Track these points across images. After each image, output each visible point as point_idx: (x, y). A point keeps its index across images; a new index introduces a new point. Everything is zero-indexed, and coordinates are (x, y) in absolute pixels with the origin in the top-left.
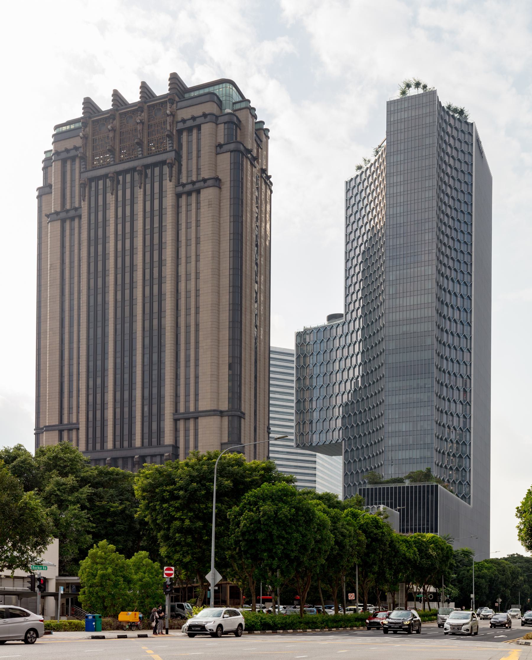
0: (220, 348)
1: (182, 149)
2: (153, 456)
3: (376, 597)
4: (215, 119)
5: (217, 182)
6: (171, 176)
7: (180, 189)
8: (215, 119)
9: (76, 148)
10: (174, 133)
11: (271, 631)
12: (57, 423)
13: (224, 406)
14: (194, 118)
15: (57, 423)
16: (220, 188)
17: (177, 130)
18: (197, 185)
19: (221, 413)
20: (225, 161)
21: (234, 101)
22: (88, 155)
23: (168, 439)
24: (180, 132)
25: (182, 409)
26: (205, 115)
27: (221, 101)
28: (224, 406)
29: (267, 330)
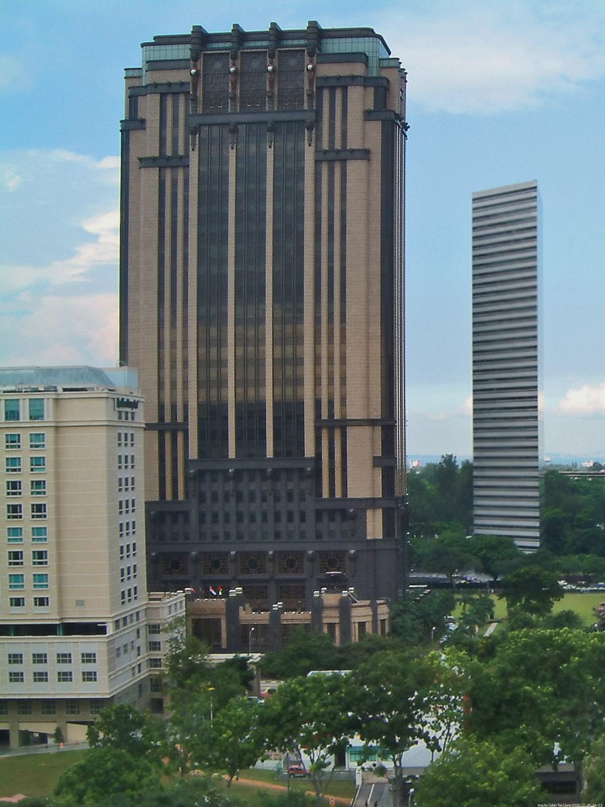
0: (370, 345)
1: (322, 107)
2: (289, 471)
3: (381, 597)
4: (365, 81)
5: (365, 154)
6: (310, 140)
7: (321, 156)
8: (365, 81)
9: (182, 84)
10: (315, 91)
11: (99, 625)
12: (156, 422)
13: (377, 414)
14: (339, 78)
15: (156, 422)
16: (369, 160)
17: (317, 87)
18: (342, 155)
19: (372, 423)
20: (375, 130)
21: (380, 57)
22: (198, 95)
23: (309, 451)
24: (320, 89)
25: (325, 416)
26: (353, 78)
27: (367, 57)
28: (377, 414)
29: (124, 193)
